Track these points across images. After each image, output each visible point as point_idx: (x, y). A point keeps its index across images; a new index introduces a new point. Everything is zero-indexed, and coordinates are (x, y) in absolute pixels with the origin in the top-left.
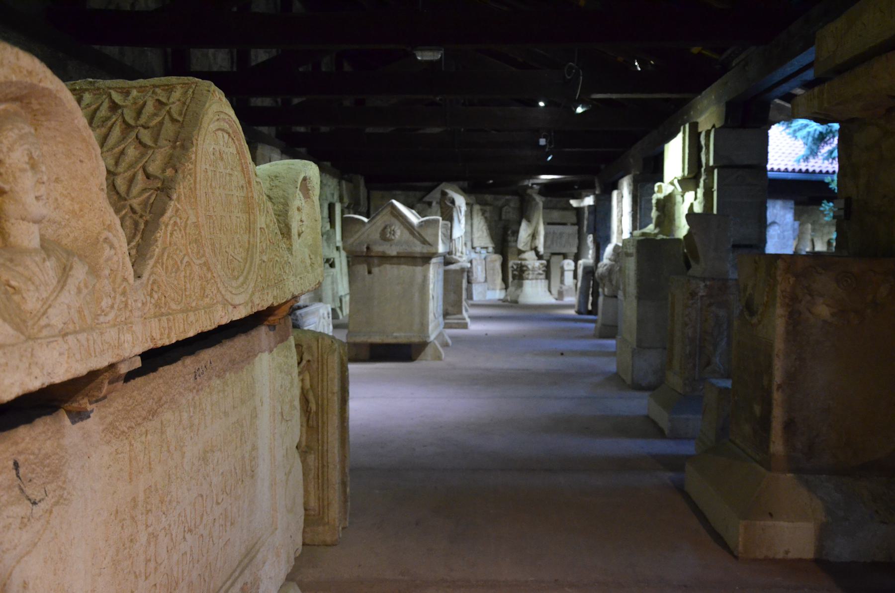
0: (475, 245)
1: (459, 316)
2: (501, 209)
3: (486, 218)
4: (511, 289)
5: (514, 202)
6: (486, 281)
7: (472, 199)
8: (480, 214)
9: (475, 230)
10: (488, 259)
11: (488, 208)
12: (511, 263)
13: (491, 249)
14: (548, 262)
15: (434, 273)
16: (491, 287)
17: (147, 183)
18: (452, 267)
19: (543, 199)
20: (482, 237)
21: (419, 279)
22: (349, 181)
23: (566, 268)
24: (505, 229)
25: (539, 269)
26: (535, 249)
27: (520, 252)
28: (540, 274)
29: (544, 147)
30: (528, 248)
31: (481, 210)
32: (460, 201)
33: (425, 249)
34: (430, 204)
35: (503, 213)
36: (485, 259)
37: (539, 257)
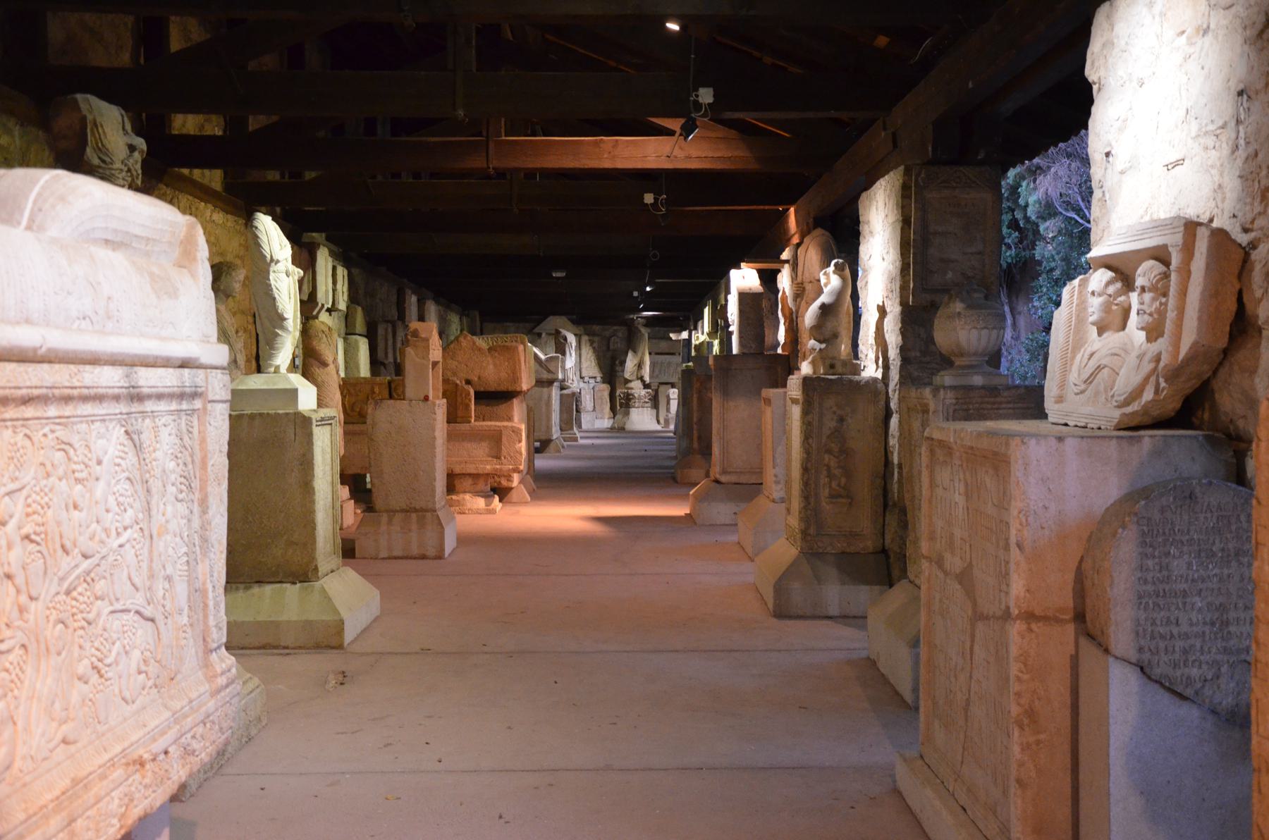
0: (583, 375)
1: (572, 432)
2: (609, 340)
3: (594, 348)
4: (619, 417)
5: (621, 332)
6: (594, 410)
7: (580, 330)
8: (588, 344)
9: (583, 360)
10: (596, 389)
11: (596, 339)
12: (619, 391)
13: (599, 379)
14: (656, 392)
15: (555, 392)
16: (600, 416)
17: (1204, 481)
18: (565, 392)
19: (649, 330)
20: (591, 367)
21: (546, 397)
22: (468, 316)
23: (671, 397)
24: (613, 359)
25: (645, 397)
26: (641, 379)
27: (627, 381)
28: (645, 402)
29: (638, 297)
30: (635, 378)
31: (590, 340)
32: (571, 339)
33: (550, 376)
34: (539, 335)
35: (611, 344)
36: (593, 388)
37: (646, 386)
